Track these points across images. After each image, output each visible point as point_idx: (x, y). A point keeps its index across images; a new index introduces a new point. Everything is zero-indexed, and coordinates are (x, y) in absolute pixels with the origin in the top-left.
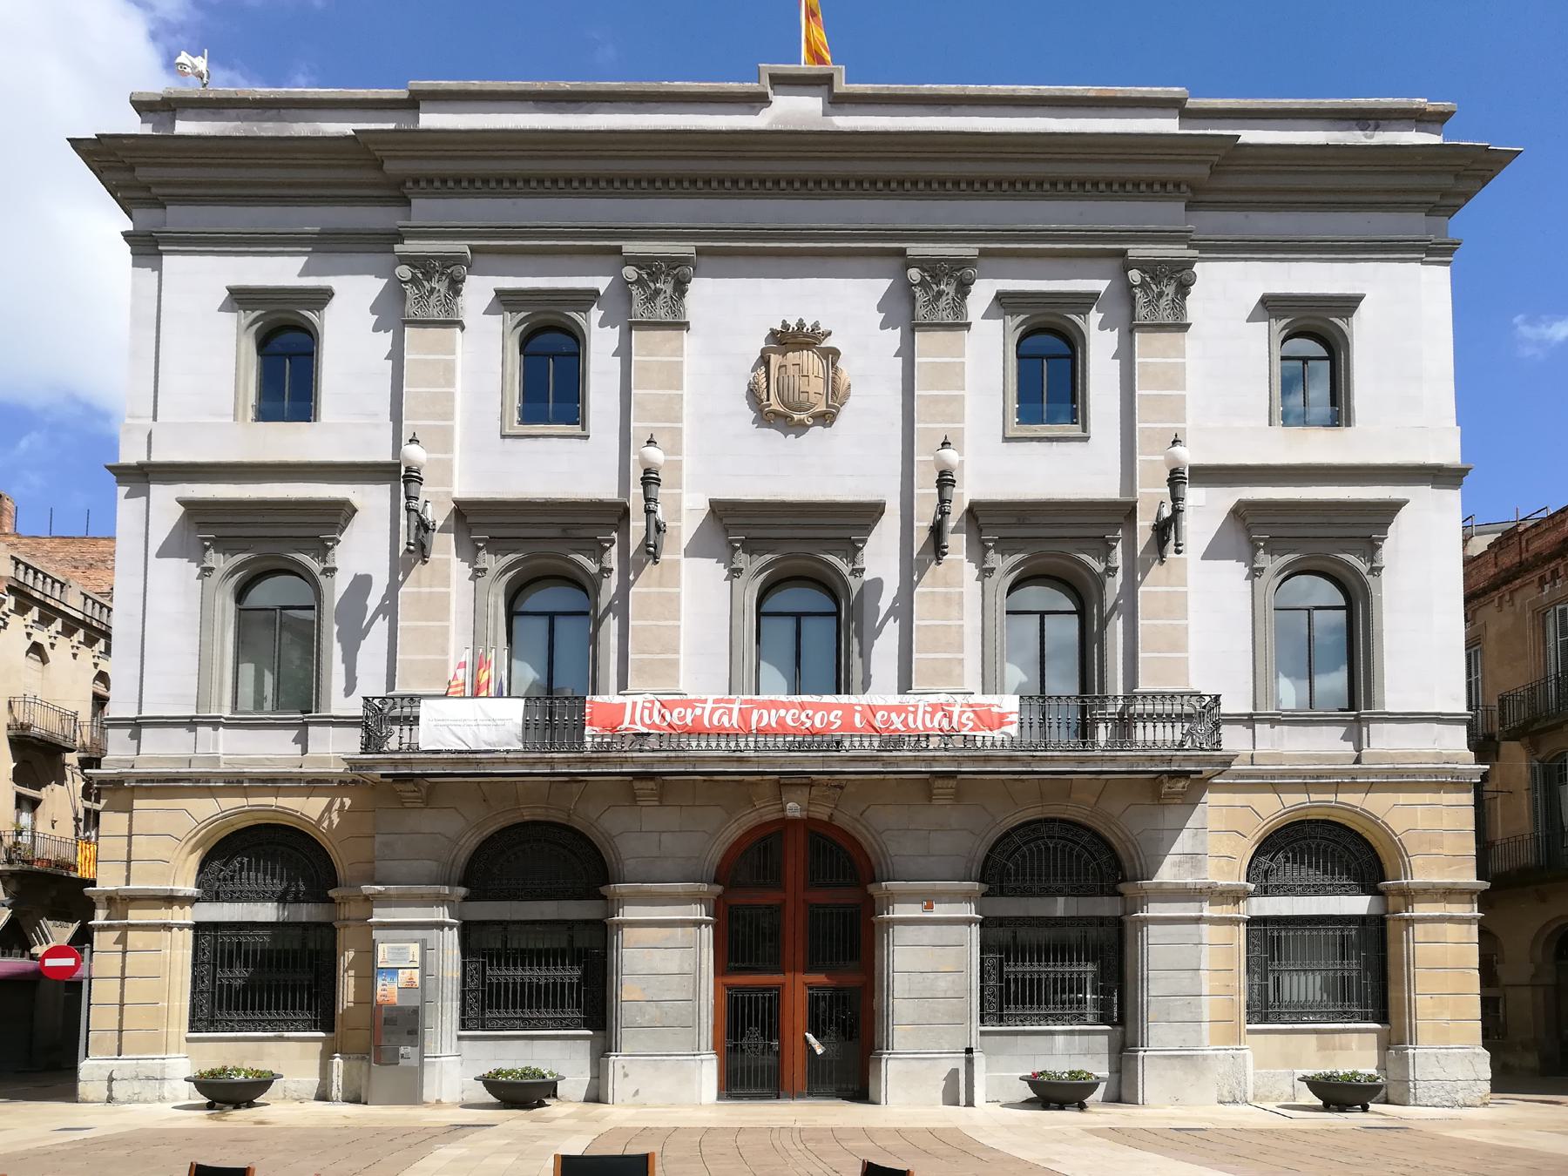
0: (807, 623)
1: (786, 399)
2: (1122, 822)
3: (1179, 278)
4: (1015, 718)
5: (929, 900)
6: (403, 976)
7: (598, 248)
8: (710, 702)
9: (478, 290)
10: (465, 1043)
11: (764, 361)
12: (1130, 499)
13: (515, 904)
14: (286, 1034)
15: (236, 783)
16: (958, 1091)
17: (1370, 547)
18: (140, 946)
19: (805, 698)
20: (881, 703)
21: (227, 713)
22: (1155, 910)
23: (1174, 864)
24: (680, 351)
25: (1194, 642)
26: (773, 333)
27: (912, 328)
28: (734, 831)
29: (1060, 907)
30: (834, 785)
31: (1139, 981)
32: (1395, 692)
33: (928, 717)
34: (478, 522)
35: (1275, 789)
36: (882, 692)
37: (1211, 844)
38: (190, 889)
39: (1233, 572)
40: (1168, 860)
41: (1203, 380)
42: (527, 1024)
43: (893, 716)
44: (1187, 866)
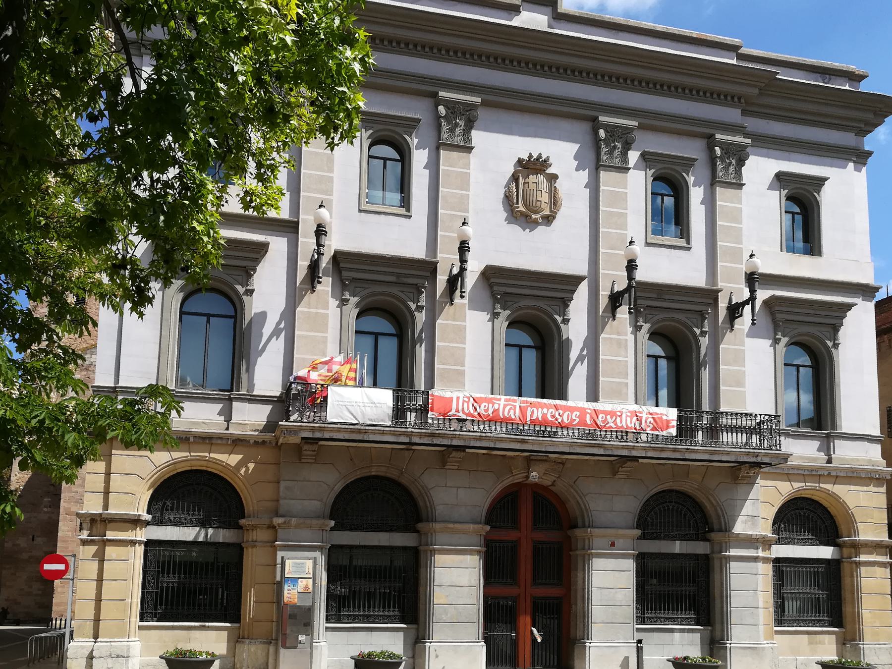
0: (382, 341)
1: (526, 206)
4: (675, 423)
6: (302, 584)
7: (426, 89)
8: (503, 400)
10: (329, 633)
11: (515, 178)
12: (434, 260)
13: (363, 534)
14: (207, 624)
17: (835, 328)
18: (114, 556)
19: (545, 401)
20: (602, 409)
24: (468, 166)
25: (748, 381)
26: (520, 161)
27: (598, 167)
28: (499, 488)
29: (677, 547)
30: (559, 461)
31: (724, 598)
33: (629, 419)
37: (757, 510)
40: (740, 520)
42: (367, 619)
43: (609, 417)
44: (750, 523)
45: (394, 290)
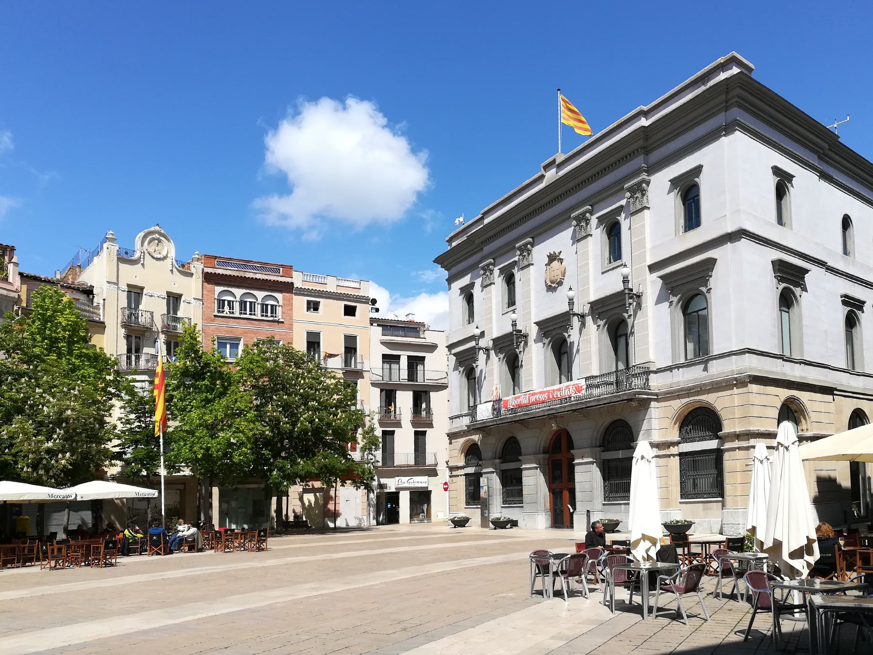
21: (682, 361)
23: (644, 434)
37: (659, 423)
38: (676, 438)
40: (641, 433)
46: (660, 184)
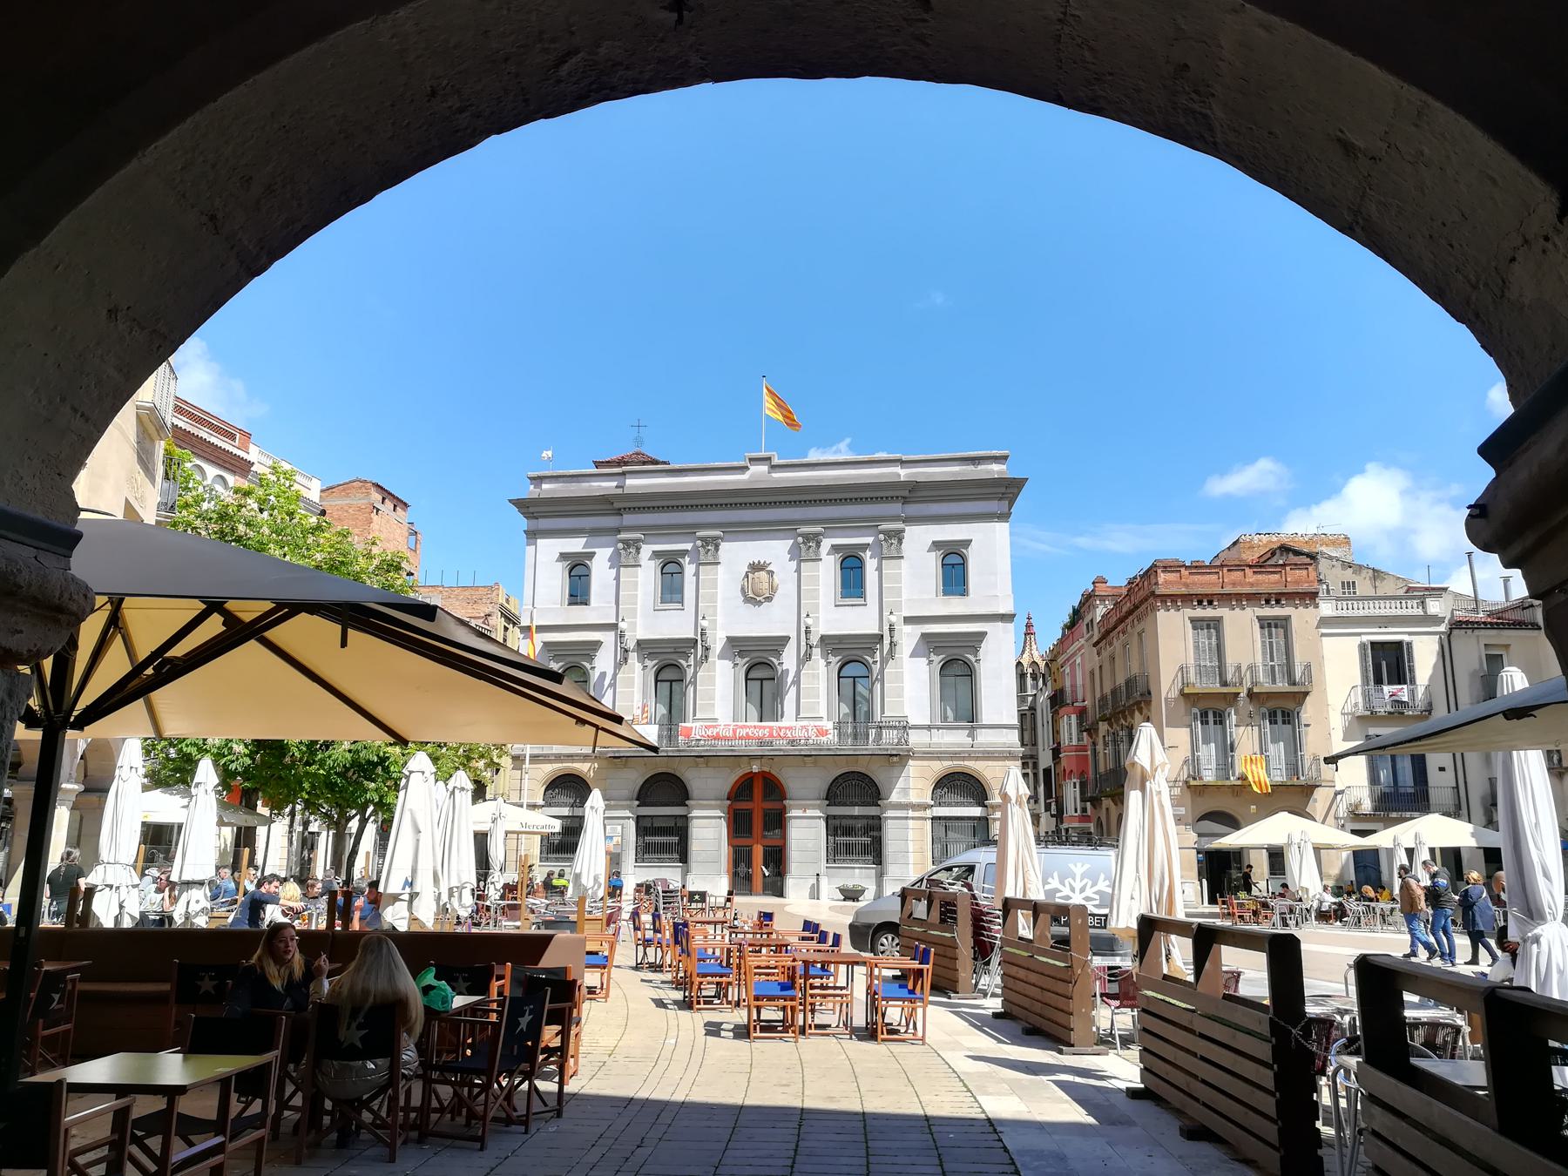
2: (879, 776)
3: (898, 535)
5: (805, 808)
7: (688, 530)
9: (647, 550)
15: (559, 758)
16: (815, 894)
17: (975, 651)
22: (890, 813)
29: (857, 811)
32: (987, 714)
34: (646, 648)
35: (939, 759)
36: (788, 720)
37: (912, 785)
39: (728, 664)
41: (909, 579)
42: (661, 860)
45: (674, 656)
46: (920, 539)
